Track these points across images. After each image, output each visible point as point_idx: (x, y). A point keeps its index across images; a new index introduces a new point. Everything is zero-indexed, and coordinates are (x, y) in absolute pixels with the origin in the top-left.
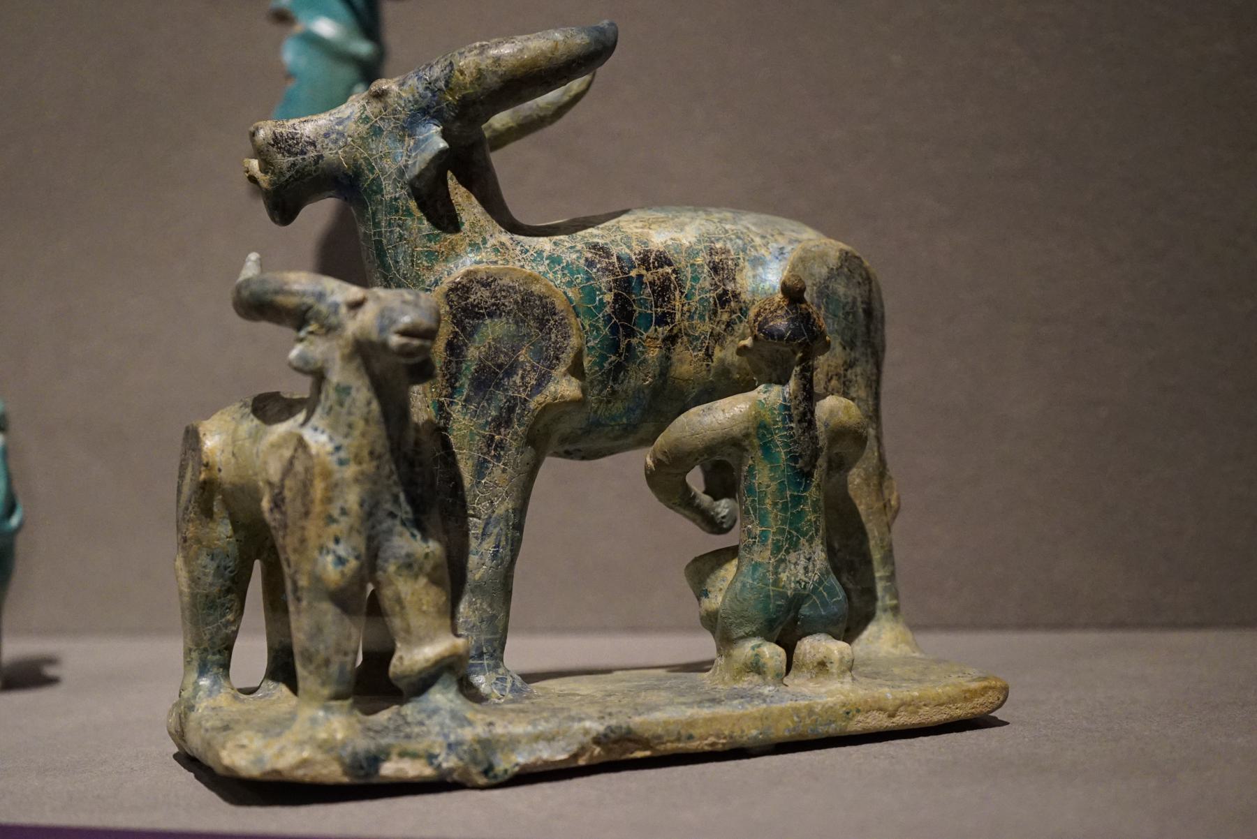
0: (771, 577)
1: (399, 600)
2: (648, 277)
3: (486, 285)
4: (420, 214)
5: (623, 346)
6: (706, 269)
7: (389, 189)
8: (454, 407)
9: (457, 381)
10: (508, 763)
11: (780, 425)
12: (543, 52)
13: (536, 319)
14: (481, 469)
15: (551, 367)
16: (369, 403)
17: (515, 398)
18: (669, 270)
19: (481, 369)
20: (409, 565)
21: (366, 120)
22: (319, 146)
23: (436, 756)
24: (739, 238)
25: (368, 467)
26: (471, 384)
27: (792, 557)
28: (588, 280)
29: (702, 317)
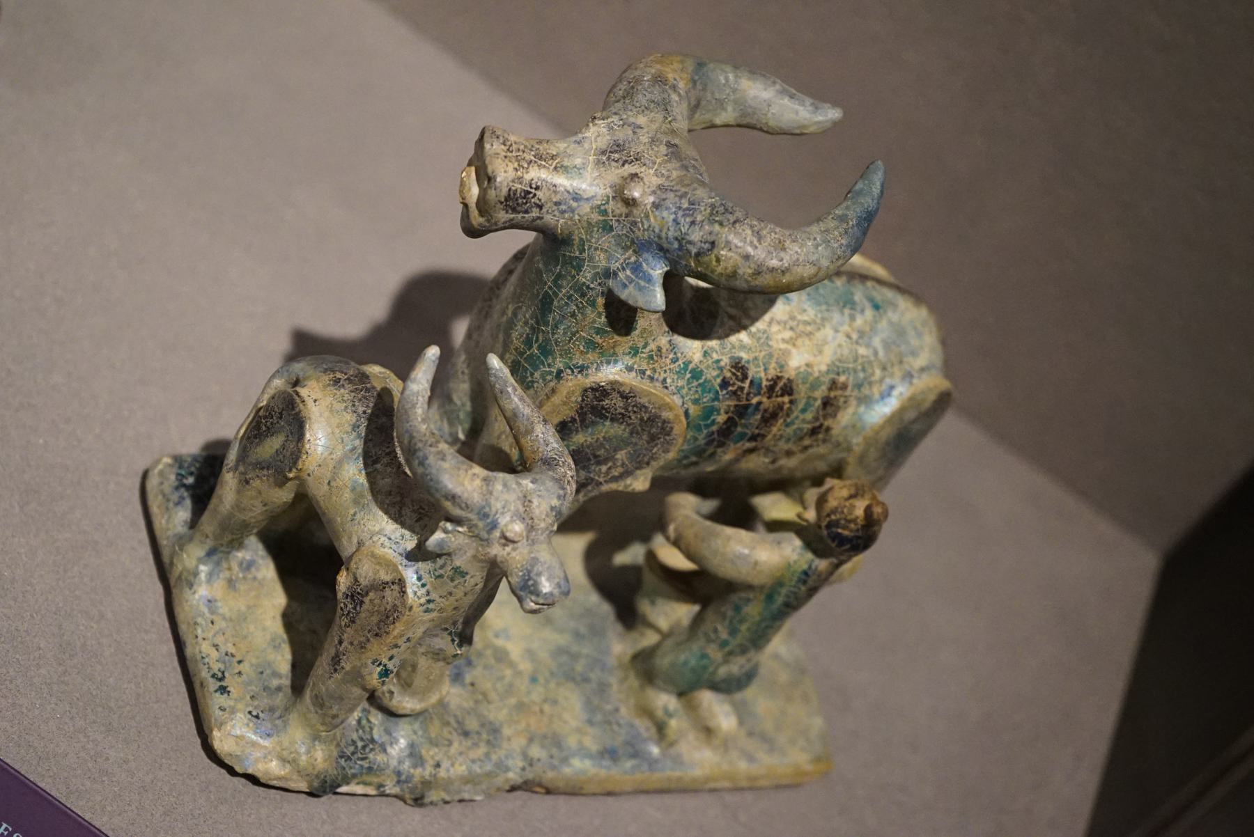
3: (624, 397)
4: (601, 310)
6: (819, 402)
17: (592, 479)
18: (786, 399)
21: (605, 213)
22: (544, 210)
24: (864, 370)
28: (713, 400)
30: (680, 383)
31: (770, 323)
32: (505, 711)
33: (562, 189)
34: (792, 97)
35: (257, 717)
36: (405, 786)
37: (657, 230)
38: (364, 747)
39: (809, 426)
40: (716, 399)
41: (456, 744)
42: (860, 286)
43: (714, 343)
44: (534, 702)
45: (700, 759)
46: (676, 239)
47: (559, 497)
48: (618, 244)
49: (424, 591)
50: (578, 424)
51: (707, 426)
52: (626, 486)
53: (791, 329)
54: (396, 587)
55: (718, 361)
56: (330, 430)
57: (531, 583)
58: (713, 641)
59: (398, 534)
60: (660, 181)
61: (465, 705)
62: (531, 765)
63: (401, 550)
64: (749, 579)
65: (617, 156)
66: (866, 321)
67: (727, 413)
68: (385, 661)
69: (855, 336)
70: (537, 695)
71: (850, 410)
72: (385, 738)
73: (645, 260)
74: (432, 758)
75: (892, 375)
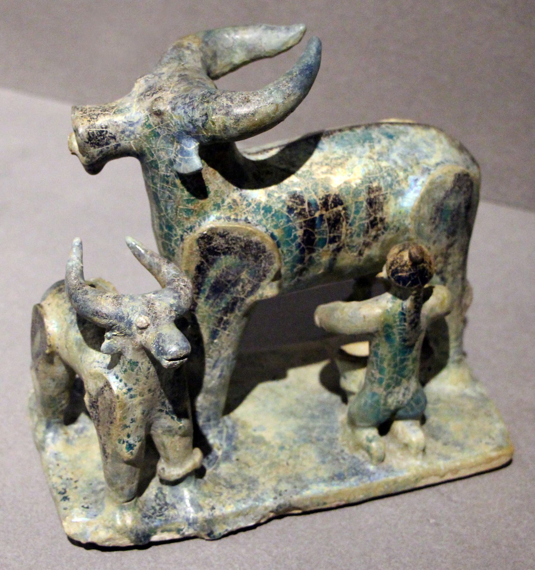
0: (382, 402)
1: (163, 445)
2: (326, 214)
3: (223, 236)
4: (182, 187)
5: (307, 257)
6: (365, 204)
7: (163, 169)
8: (199, 300)
9: (202, 286)
10: (219, 530)
11: (398, 323)
12: (268, 115)
13: (253, 256)
14: (214, 334)
15: (261, 280)
16: (149, 369)
17: (236, 298)
18: (340, 208)
19: (217, 282)
20: (170, 431)
21: (149, 126)
22: (118, 139)
23: (182, 530)
24: (389, 175)
25: (148, 396)
26: (210, 289)
27: (397, 389)
29: (358, 235)
30: (259, 218)
31: (311, 166)
32: (261, 469)
33: (121, 122)
34: (272, 29)
35: (88, 508)
36: (195, 526)
37: (179, 123)
38: (161, 509)
39: (367, 221)
40: (289, 221)
41: (225, 494)
42: (376, 129)
43: (273, 188)
44: (283, 460)
45: (407, 467)
46: (189, 122)
47: (175, 298)
48: (167, 142)
49: (122, 384)
50: (206, 265)
51: (293, 240)
52: (261, 296)
53: (327, 164)
54: (107, 388)
55: (279, 197)
56: (58, 317)
57: (160, 348)
58: (374, 382)
59: (102, 357)
60: (173, 95)
61: (232, 472)
62: (280, 495)
63: (104, 365)
64: (365, 328)
65: (149, 93)
66: (383, 147)
67: (301, 228)
68: (126, 439)
69: (375, 157)
70: (284, 456)
71: (392, 203)
72: (174, 500)
73: (184, 144)
74: (208, 504)
75: (413, 173)
